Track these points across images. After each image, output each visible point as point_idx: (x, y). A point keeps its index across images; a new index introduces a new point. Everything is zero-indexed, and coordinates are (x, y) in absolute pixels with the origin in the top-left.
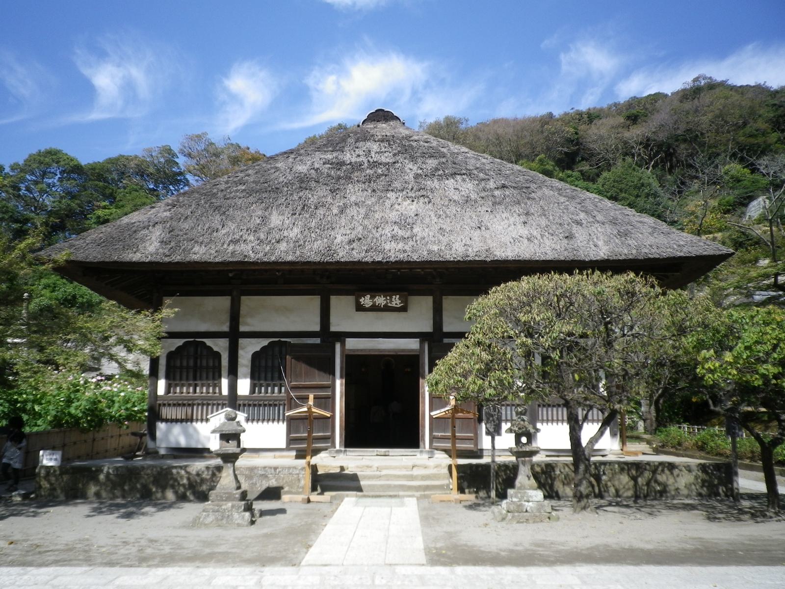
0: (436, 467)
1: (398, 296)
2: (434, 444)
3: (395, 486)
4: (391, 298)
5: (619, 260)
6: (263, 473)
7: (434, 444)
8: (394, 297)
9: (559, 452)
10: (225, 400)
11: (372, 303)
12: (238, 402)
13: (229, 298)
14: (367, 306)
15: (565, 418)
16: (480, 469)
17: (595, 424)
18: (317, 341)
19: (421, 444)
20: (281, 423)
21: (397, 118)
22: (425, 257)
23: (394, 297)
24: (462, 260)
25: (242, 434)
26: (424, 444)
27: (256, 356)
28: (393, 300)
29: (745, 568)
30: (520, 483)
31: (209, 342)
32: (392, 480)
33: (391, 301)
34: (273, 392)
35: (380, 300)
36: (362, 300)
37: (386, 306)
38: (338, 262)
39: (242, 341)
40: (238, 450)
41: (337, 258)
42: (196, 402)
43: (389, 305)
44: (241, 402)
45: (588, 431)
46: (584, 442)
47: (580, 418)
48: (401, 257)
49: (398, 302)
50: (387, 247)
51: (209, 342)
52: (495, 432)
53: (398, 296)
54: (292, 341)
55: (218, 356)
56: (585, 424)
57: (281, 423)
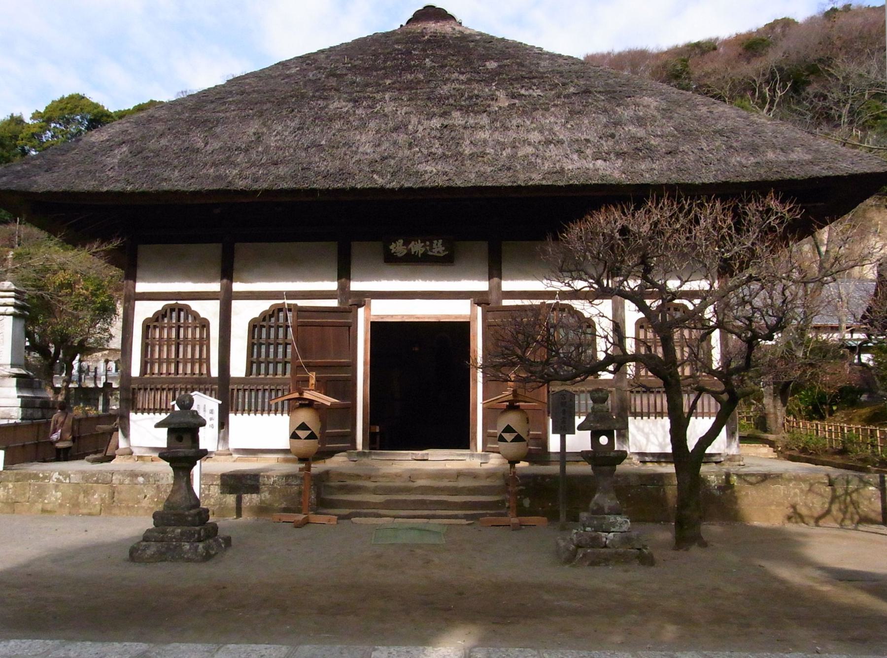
0: (488, 477)
1: (441, 241)
2: (489, 446)
3: (432, 502)
4: (432, 243)
5: (741, 183)
6: (253, 483)
7: (489, 446)
8: (435, 242)
9: (660, 458)
10: (215, 384)
11: (405, 251)
12: (231, 387)
13: (220, 245)
14: (399, 255)
15: (666, 409)
16: (547, 480)
17: (706, 418)
18: (333, 303)
19: (472, 445)
20: (286, 415)
21: (452, 18)
22: (473, 181)
23: (435, 242)
24: (523, 184)
25: (201, 429)
26: (476, 445)
27: (255, 326)
28: (434, 246)
29: (259, 244)
30: (597, 504)
31: (194, 305)
32: (427, 494)
33: (432, 249)
34: (267, 373)
35: (417, 247)
36: (392, 247)
37: (424, 254)
38: (353, 190)
39: (235, 304)
40: (191, 452)
41: (351, 183)
42: (178, 386)
43: (430, 253)
44: (235, 387)
45: (698, 427)
46: (691, 444)
47: (686, 409)
48: (441, 181)
49: (441, 249)
50: (422, 168)
51: (194, 305)
52: (565, 428)
53: (441, 241)
54: (301, 303)
55: (205, 324)
56: (692, 419)
57: (286, 415)
